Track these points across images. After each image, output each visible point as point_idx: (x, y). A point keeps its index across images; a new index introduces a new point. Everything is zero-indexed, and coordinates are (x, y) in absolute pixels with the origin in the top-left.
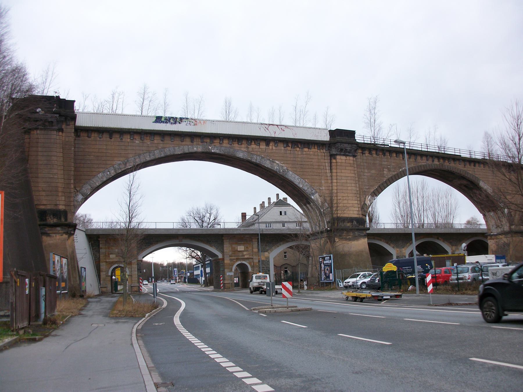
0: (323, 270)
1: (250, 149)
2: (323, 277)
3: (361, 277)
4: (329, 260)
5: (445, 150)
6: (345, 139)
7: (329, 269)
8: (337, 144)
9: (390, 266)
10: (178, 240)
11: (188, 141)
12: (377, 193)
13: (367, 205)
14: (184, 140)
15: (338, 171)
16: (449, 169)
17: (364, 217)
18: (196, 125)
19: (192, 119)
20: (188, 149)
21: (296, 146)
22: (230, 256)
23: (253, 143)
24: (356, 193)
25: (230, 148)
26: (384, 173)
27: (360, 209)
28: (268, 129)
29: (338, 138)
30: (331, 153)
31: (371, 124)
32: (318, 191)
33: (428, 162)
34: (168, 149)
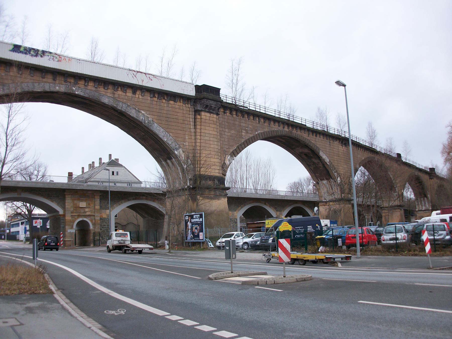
0: (190, 229)
1: (116, 96)
2: (190, 236)
3: (235, 237)
4: (198, 218)
5: (294, 118)
6: (211, 96)
7: (198, 228)
8: (203, 100)
9: (286, 226)
10: (16, 193)
11: (49, 78)
12: (235, 153)
13: (227, 164)
14: (45, 76)
15: (202, 127)
16: (296, 137)
17: (224, 176)
18: (60, 61)
19: (56, 54)
20: (50, 88)
21: (162, 98)
22: (72, 213)
23: (120, 89)
24: (218, 151)
25: (96, 91)
26: (243, 134)
27: (221, 168)
28: (135, 76)
29: (205, 94)
30: (196, 109)
31: (233, 85)
32: (182, 146)
33: (279, 128)
34: (26, 85)
